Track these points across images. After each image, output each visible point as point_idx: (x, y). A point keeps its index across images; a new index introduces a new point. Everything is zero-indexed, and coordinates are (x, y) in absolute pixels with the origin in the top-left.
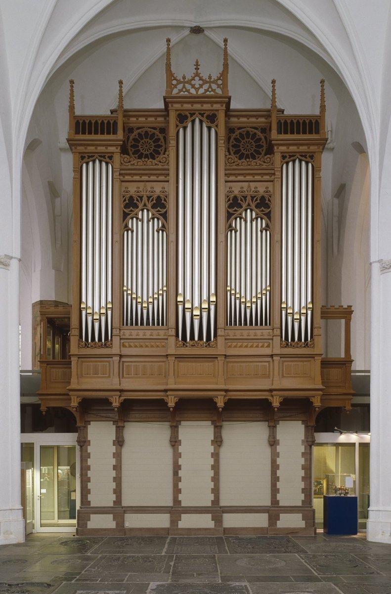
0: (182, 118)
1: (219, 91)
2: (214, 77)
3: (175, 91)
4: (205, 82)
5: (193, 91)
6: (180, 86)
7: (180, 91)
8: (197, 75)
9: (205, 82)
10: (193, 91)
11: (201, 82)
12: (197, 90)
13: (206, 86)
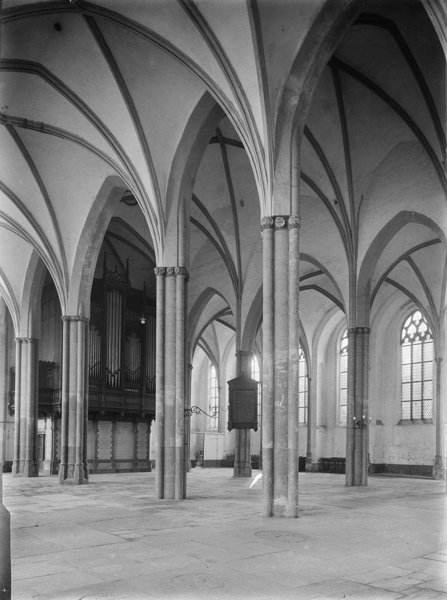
6: (109, 274)
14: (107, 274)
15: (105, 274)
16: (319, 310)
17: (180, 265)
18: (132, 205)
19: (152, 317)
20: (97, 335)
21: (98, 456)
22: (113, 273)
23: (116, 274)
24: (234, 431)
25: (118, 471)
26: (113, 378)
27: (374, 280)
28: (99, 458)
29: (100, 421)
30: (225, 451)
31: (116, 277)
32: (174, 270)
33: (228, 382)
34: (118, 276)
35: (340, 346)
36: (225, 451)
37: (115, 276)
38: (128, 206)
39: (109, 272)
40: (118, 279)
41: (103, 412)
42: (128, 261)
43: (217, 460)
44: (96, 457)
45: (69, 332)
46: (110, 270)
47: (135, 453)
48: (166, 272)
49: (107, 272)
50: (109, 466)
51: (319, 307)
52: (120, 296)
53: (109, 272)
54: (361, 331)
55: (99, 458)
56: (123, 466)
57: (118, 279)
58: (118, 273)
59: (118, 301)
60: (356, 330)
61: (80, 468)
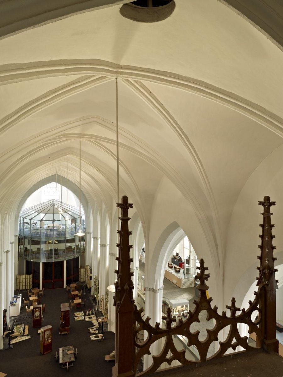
4: (222, 321)
9: (222, 321)
13: (223, 334)
40: (214, 348)
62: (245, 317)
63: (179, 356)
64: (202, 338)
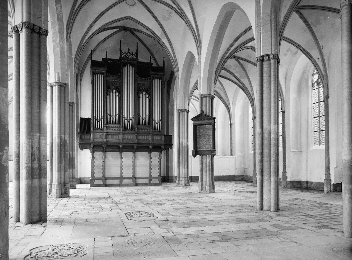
0: (125, 65)
1: (135, 57)
2: (134, 53)
3: (122, 56)
4: (131, 54)
5: (128, 57)
6: (124, 55)
7: (131, 57)
8: (129, 52)
9: (131, 54)
10: (128, 57)
11: (130, 54)
12: (129, 56)
14: (123, 55)
15: (121, 55)
16: (287, 54)
17: (24, 21)
18: (132, 6)
19: (157, 80)
20: (117, 96)
21: (152, 174)
22: (127, 54)
23: (129, 54)
24: (198, 156)
25: (137, 185)
26: (128, 123)
27: (285, 6)
28: (95, 177)
29: (152, 152)
30: (236, 169)
31: (129, 56)
32: (17, 28)
33: (193, 119)
34: (130, 56)
35: (312, 81)
36: (236, 169)
37: (128, 55)
38: (131, 7)
39: (124, 54)
40: (130, 57)
41: (151, 147)
42: (137, 44)
43: (229, 176)
44: (121, 176)
45: (53, 94)
46: (124, 52)
47: (150, 173)
48: (263, 59)
49: (122, 54)
50: (100, 182)
51: (287, 51)
52: (133, 68)
53: (124, 54)
54: (267, 58)
55: (95, 177)
56: (125, 181)
57: (130, 57)
58: (130, 53)
59: (131, 71)
60: (262, 58)
61: (185, 179)
62: (134, 55)
63: (134, 57)
64: (129, 55)
